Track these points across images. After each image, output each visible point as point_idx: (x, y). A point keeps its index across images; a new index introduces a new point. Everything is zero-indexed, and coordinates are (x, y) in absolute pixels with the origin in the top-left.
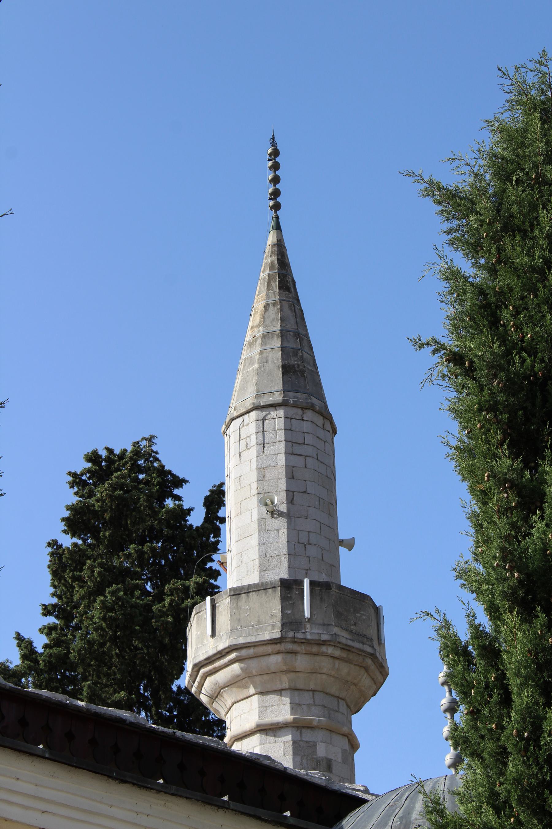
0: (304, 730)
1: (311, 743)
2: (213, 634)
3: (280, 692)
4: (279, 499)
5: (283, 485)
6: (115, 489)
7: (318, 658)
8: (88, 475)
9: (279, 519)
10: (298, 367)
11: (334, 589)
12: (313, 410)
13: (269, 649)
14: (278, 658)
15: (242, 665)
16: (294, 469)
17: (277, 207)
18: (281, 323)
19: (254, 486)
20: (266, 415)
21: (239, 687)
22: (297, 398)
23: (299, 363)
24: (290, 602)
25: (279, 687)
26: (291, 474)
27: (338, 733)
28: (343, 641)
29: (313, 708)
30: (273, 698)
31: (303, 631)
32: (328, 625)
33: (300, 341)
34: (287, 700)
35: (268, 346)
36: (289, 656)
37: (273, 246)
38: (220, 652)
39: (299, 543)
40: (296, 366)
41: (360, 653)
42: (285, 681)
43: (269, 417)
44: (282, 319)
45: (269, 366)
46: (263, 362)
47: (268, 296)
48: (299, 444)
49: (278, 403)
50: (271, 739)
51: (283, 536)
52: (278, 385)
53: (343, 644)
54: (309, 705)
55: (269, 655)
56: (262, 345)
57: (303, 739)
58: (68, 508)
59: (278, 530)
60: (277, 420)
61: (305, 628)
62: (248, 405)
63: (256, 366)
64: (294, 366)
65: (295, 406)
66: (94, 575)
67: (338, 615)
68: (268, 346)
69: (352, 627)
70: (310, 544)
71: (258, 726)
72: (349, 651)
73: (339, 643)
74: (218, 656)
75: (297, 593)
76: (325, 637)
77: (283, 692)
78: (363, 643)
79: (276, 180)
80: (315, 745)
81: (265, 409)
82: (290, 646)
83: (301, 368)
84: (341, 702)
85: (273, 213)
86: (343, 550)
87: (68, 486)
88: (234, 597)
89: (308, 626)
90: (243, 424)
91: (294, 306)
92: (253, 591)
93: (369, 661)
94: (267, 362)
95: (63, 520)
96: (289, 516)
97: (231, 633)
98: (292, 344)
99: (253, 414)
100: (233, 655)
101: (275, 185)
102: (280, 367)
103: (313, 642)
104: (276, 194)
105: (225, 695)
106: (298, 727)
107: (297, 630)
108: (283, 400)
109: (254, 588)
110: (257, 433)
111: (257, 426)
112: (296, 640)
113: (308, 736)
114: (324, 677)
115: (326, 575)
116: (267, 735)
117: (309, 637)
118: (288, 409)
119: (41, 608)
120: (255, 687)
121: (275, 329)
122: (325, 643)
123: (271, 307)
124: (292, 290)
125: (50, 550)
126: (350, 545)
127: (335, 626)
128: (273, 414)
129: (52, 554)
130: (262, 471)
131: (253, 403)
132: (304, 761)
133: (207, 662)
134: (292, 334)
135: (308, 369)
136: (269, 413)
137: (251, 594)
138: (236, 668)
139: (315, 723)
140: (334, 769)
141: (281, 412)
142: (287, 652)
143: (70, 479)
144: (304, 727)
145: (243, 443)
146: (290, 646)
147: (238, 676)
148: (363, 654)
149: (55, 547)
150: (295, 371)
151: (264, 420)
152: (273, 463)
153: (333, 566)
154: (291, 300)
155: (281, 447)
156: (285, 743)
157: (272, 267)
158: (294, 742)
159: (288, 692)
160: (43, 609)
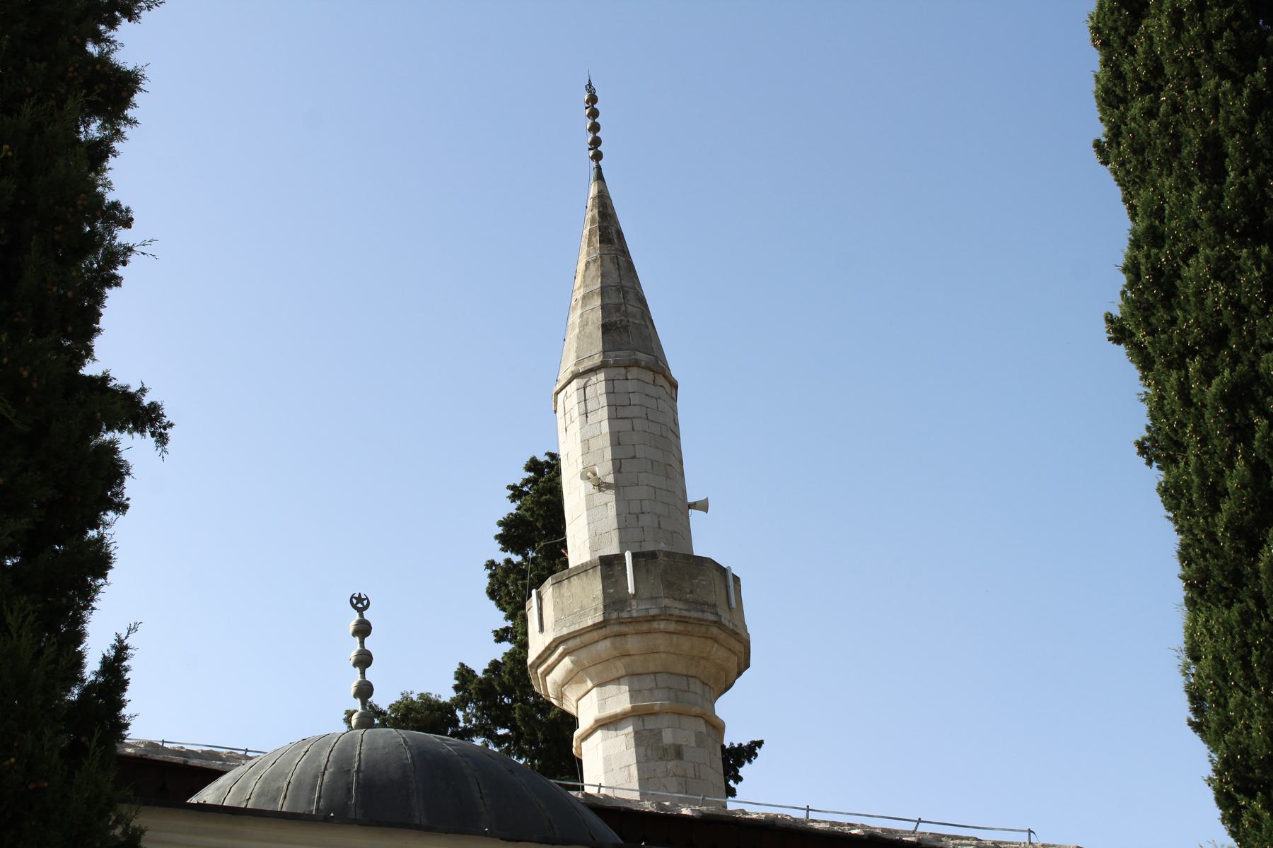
0: (646, 718)
2: (542, 629)
3: (617, 680)
4: (605, 470)
5: (608, 454)
6: (542, 494)
7: (650, 636)
11: (661, 557)
13: (595, 635)
14: (607, 643)
17: (598, 156)
19: (580, 460)
21: (577, 683)
26: (617, 440)
28: (676, 612)
29: (656, 692)
30: (611, 689)
36: (618, 639)
37: (594, 199)
38: (548, 648)
42: (620, 668)
46: (584, 325)
47: (588, 254)
50: (612, 733)
51: (612, 510)
52: (598, 346)
54: (651, 690)
58: (500, 524)
65: (617, 365)
67: (669, 585)
71: (597, 721)
76: (653, 612)
78: (703, 611)
79: (595, 128)
80: (659, 732)
82: (616, 629)
85: (594, 164)
86: (694, 515)
87: (509, 501)
89: (634, 602)
90: (566, 397)
93: (715, 631)
95: (496, 537)
96: (617, 487)
98: (614, 299)
99: (574, 384)
100: (561, 649)
104: (596, 142)
107: (622, 610)
113: (651, 723)
114: (663, 656)
117: (635, 615)
118: (609, 370)
122: (654, 618)
125: (489, 571)
126: (703, 506)
128: (594, 379)
129: (491, 576)
130: (586, 442)
132: (649, 752)
138: (567, 661)
139: (657, 708)
140: (686, 756)
141: (601, 376)
143: (510, 492)
146: (616, 629)
147: (571, 671)
151: (585, 388)
155: (604, 413)
156: (626, 735)
158: (636, 733)
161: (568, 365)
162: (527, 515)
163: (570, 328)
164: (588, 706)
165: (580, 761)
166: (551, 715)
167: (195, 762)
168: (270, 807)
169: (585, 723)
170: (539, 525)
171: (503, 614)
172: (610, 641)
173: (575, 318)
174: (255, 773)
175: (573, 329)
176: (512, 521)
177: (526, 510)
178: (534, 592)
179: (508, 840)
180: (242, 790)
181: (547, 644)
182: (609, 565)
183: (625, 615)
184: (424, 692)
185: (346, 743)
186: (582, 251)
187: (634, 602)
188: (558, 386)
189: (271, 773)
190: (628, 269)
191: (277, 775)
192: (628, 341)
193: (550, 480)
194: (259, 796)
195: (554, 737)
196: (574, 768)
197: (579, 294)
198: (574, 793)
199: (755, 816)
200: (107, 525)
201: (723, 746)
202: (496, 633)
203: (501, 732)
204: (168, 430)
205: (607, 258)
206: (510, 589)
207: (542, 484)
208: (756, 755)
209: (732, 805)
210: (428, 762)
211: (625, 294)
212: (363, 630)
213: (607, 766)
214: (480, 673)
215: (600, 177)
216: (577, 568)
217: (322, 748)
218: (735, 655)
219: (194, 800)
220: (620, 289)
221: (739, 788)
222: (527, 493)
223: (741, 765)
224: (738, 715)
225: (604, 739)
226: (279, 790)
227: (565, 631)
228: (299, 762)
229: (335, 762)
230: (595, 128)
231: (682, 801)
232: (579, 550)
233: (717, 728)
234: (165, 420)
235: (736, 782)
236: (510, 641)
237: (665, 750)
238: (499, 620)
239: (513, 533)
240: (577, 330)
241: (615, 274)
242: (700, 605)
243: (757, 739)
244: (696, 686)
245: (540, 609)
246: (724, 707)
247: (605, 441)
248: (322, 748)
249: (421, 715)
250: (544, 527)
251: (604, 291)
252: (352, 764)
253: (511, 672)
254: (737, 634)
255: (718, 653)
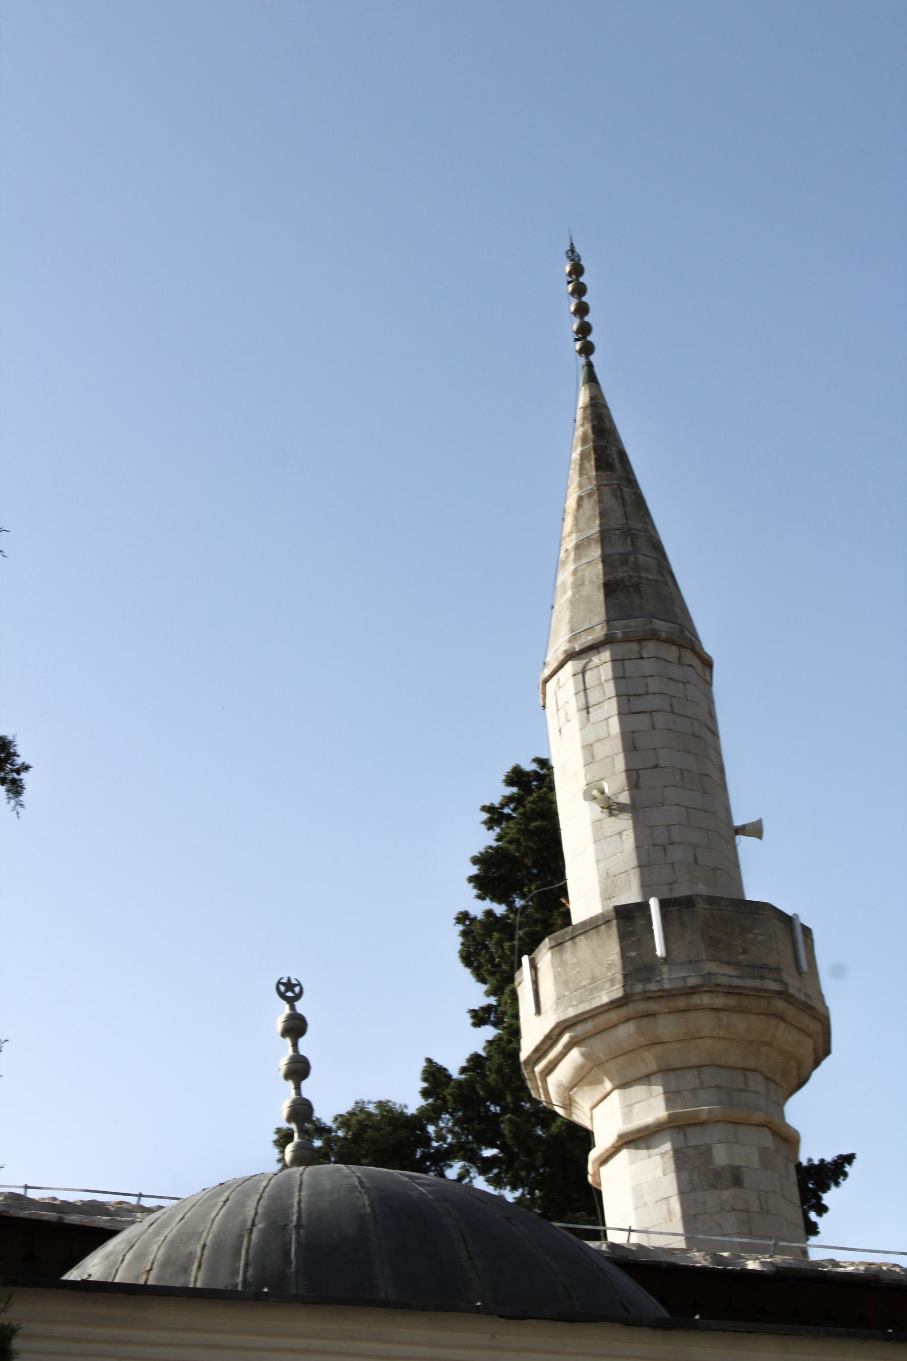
0: (689, 1130)
1: (703, 1148)
2: (538, 1011)
3: (646, 1079)
4: (616, 785)
5: (620, 763)
7: (691, 1015)
8: (512, 806)
9: (621, 816)
10: (630, 580)
11: (701, 906)
12: (658, 640)
13: (613, 1016)
15: (583, 1049)
16: (635, 735)
17: (587, 349)
18: (601, 520)
20: (587, 663)
22: (629, 627)
23: (632, 573)
24: (634, 939)
25: (643, 1071)
27: (750, 1125)
28: (725, 981)
30: (638, 1091)
31: (658, 979)
32: (697, 961)
33: (632, 541)
34: (658, 1089)
35: (584, 561)
36: (644, 1021)
37: (585, 408)
39: (654, 845)
40: (626, 580)
41: (761, 994)
42: (649, 1061)
43: (591, 665)
44: (602, 515)
45: (587, 589)
46: (578, 585)
47: (580, 486)
48: (639, 695)
49: (600, 642)
50: (643, 1153)
53: (725, 986)
54: (694, 1090)
55: (616, 1026)
56: (575, 560)
57: (690, 1144)
58: (475, 861)
59: (620, 833)
60: (602, 666)
61: (661, 974)
62: (561, 656)
63: (569, 593)
64: (622, 580)
65: (627, 639)
66: (505, 954)
67: (713, 943)
68: (584, 561)
69: (741, 957)
70: (672, 844)
71: (620, 1137)
72: (740, 994)
73: (718, 985)
74: (549, 1042)
75: (643, 922)
76: (693, 981)
77: (653, 1078)
78: (762, 978)
79: (582, 310)
81: (584, 655)
82: (642, 1006)
83: (634, 580)
84: (751, 1075)
85: (582, 360)
86: (744, 843)
88: (556, 948)
89: (665, 969)
91: (621, 490)
92: (580, 934)
94: (583, 584)
96: (635, 809)
97: (557, 1004)
98: (620, 547)
99: (570, 667)
100: (566, 1038)
101: (582, 318)
102: (601, 586)
103: (675, 992)
104: (584, 330)
105: (577, 1098)
106: (678, 1127)
107: (649, 980)
108: (606, 635)
109: (581, 928)
110: (576, 694)
111: (576, 683)
112: (649, 995)
113: (697, 1137)
114: (709, 1042)
115: (705, 885)
116: (637, 1148)
117: (667, 986)
119: (469, 1015)
120: (611, 1080)
121: (592, 532)
122: (694, 990)
123: (586, 500)
124: (618, 466)
125: (460, 927)
126: (755, 830)
127: (709, 960)
128: (596, 660)
129: (464, 934)
130: (588, 748)
131: (566, 651)
133: (539, 1054)
134: (617, 532)
135: (647, 579)
136: (591, 660)
137: (577, 939)
138: (575, 1055)
139: (704, 1116)
141: (606, 655)
142: (642, 1016)
143: (485, 816)
144: (689, 1125)
145: (562, 712)
146: (642, 1006)
148: (766, 995)
149: (467, 923)
150: (626, 587)
151: (583, 672)
152: (603, 734)
153: (718, 869)
154: (615, 482)
155: (611, 707)
156: (663, 1155)
157: (584, 440)
159: (659, 1076)
160: (473, 1017)
161: (559, 644)
162: (512, 848)
163: (559, 591)
164: (606, 1115)
165: (599, 1193)
166: (554, 1129)
167: (73, 1219)
168: (177, 1282)
169: (603, 1141)
170: (528, 861)
171: (484, 987)
172: (636, 1022)
173: (566, 576)
174: (157, 1233)
175: (564, 592)
176: (492, 856)
177: (510, 842)
178: (525, 959)
179: (510, 1318)
180: (140, 1257)
181: (547, 1030)
182: (629, 918)
183: (653, 987)
184: (383, 1098)
185: (279, 1186)
186: (572, 485)
187: (665, 969)
188: (547, 672)
189: (179, 1233)
190: (636, 504)
191: (188, 1235)
192: (642, 610)
193: (541, 799)
194: (164, 1265)
195: (559, 1161)
196: (590, 1202)
197: (570, 543)
198: (593, 1244)
199: (850, 1269)
201: (799, 1165)
202: (474, 1013)
203: (488, 1153)
204: (23, 775)
205: (607, 491)
206: (493, 952)
207: (530, 801)
208: (845, 1175)
209: (816, 1255)
210: (393, 1210)
211: (634, 538)
212: (295, 1028)
213: (638, 1202)
214: (454, 1072)
215: (591, 378)
216: (584, 924)
217: (247, 1195)
218: (815, 1040)
219: (73, 1275)
220: (627, 533)
221: (822, 1222)
222: (509, 817)
223: (826, 1188)
224: (817, 1119)
225: (632, 1162)
226: (190, 1256)
227: (571, 1012)
228: (218, 1215)
229: (266, 1214)
230: (582, 310)
231: (744, 1247)
232: (585, 898)
233: (790, 1140)
234: (19, 761)
235: (820, 1214)
236: (495, 1025)
237: (717, 1174)
238: (478, 995)
239: (492, 874)
240: (569, 591)
241: (619, 512)
242: (759, 969)
243: (846, 1152)
244: (757, 1083)
245: (535, 982)
246: (799, 1111)
247: (616, 745)
248: (247, 1195)
249: (377, 1136)
250: (535, 864)
251: (604, 537)
252: (288, 1217)
253: (499, 1071)
254: (810, 1008)
255: (785, 1036)
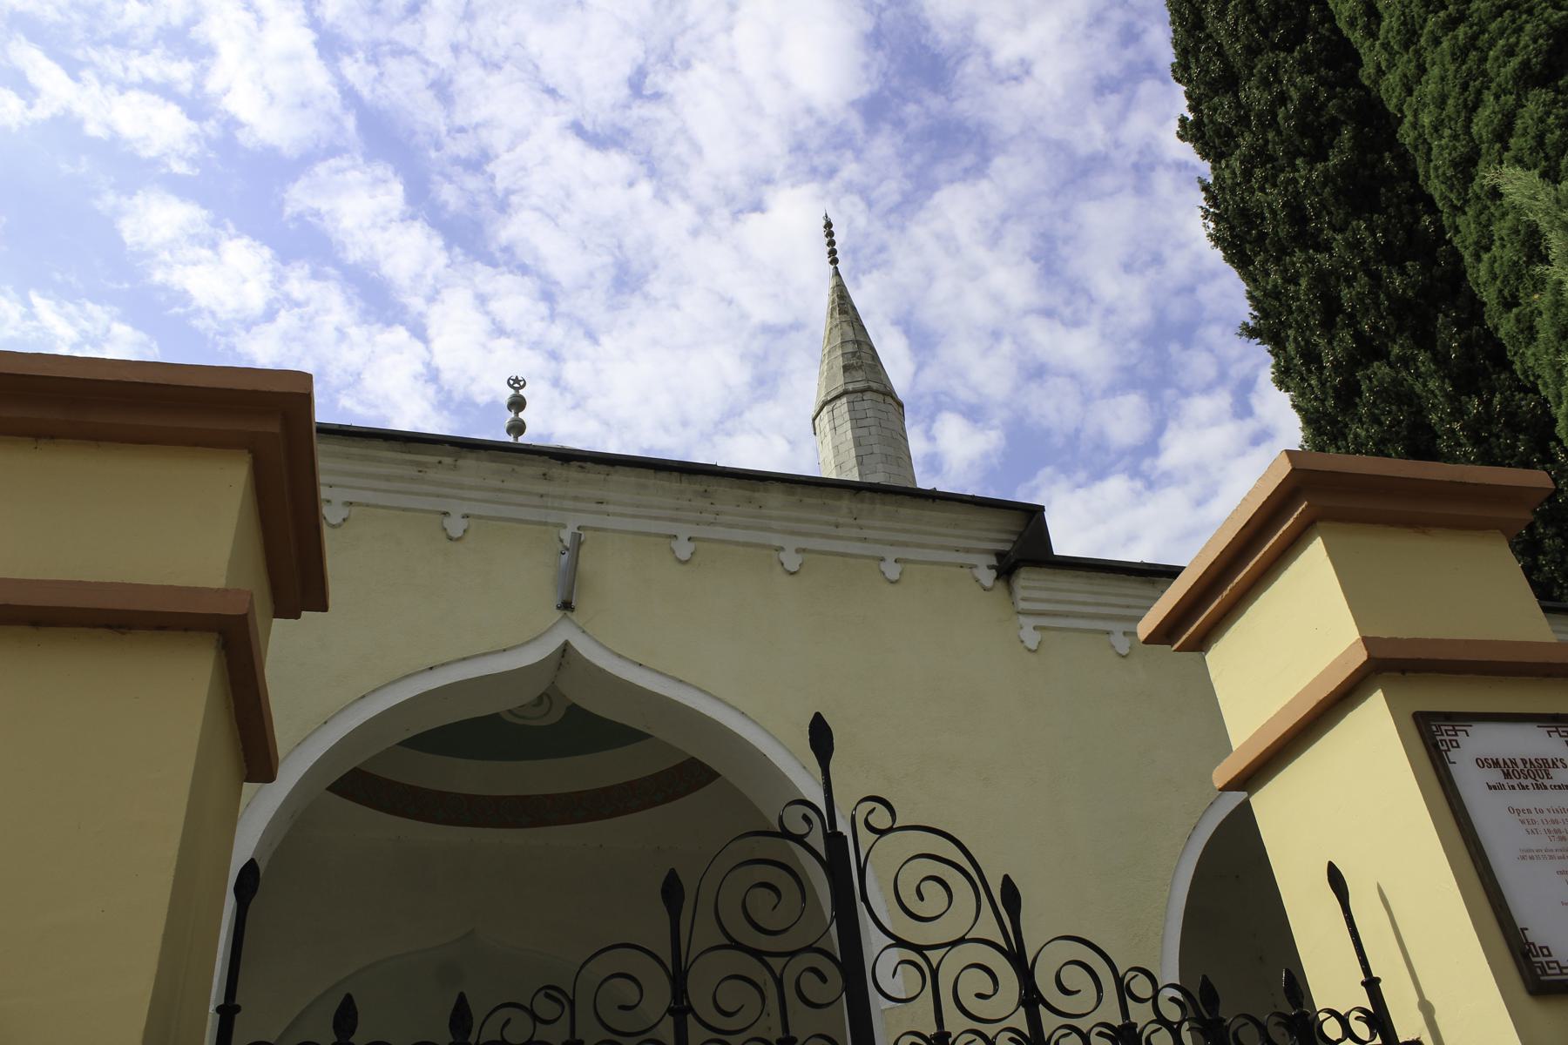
17: (834, 261)
130: (836, 447)
141: (844, 400)
200: (193, 137)
